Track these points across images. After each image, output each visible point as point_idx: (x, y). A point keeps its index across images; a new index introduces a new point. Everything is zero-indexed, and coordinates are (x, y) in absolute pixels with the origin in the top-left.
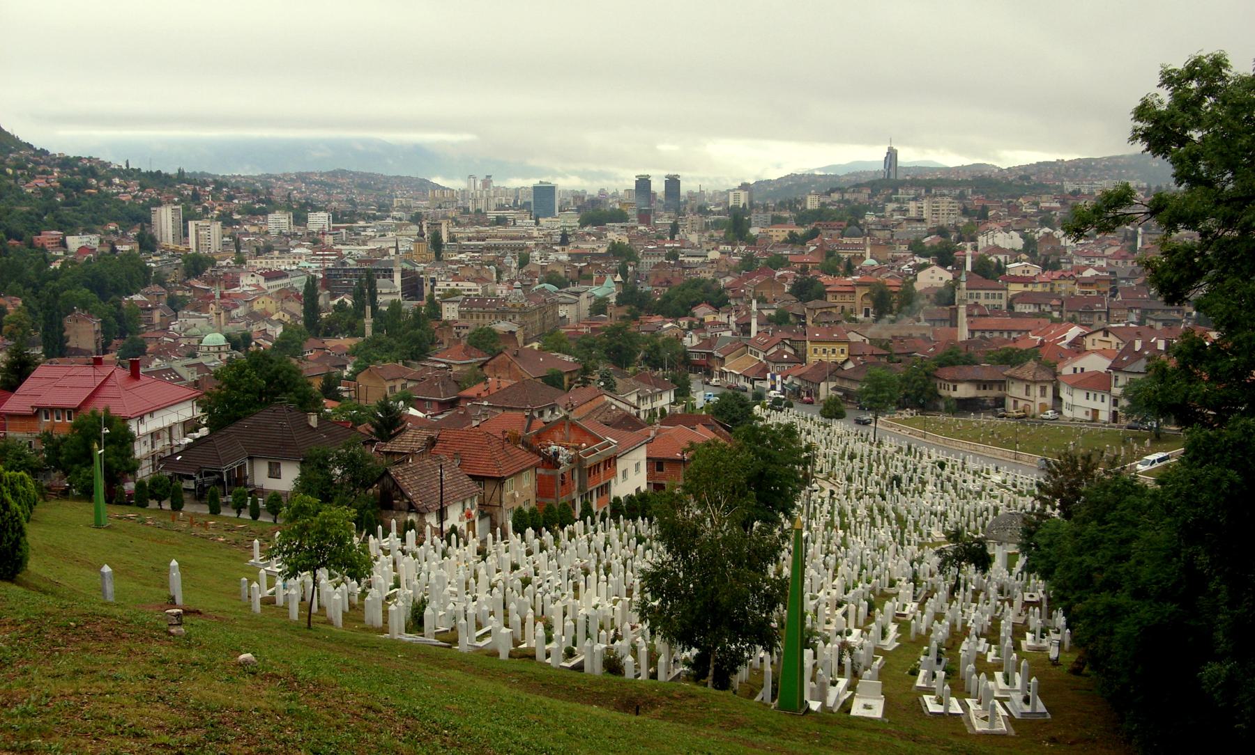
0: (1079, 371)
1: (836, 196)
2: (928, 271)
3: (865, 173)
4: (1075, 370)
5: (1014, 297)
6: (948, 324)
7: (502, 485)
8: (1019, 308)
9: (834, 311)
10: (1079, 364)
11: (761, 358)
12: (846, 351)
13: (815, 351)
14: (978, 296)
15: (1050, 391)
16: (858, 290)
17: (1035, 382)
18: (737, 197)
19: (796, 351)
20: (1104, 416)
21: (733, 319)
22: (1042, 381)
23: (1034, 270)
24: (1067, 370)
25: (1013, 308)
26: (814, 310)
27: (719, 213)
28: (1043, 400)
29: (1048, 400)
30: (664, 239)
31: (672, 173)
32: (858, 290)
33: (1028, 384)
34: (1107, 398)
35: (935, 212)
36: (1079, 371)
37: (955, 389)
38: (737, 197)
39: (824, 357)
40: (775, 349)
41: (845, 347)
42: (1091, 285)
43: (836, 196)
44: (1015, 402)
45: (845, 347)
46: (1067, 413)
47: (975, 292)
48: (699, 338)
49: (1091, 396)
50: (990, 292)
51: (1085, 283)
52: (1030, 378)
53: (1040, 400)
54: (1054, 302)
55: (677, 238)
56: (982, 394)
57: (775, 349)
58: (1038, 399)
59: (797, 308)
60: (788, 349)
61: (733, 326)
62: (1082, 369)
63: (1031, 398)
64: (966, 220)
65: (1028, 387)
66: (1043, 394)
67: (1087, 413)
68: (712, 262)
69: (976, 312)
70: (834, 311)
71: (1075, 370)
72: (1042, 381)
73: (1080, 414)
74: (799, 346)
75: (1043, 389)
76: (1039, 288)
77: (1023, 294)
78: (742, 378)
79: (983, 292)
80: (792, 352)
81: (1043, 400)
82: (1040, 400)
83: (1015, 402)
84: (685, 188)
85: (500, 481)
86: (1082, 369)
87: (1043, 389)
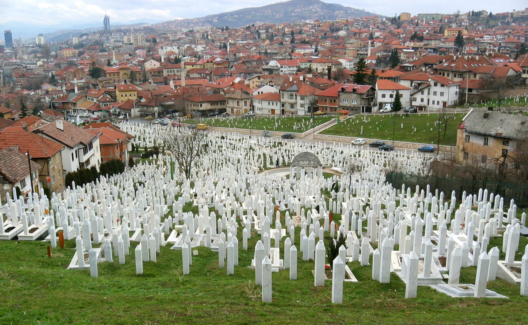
0: (260, 93)
1: (85, 37)
2: (149, 62)
3: (76, 30)
4: (259, 93)
5: (189, 72)
6: (163, 84)
7: (48, 163)
8: (192, 76)
9: (111, 81)
10: (260, 90)
11: (95, 100)
12: (136, 95)
13: (122, 96)
14: (174, 71)
15: (248, 103)
16: (120, 71)
17: (242, 99)
18: (39, 39)
19: (111, 97)
20: (278, 112)
21: (64, 88)
22: (245, 99)
23: (194, 60)
24: (255, 93)
25: (189, 76)
26: (102, 81)
27: (32, 47)
28: (245, 107)
29: (248, 107)
30: (11, 58)
31: (7, 30)
32: (120, 71)
33: (238, 101)
34: (279, 103)
35: (136, 40)
36: (260, 93)
37: (201, 106)
38: (39, 39)
39: (130, 98)
40: (102, 96)
41: (136, 93)
42: (221, 64)
43: (85, 37)
44: (232, 110)
45: (136, 93)
46: (257, 112)
47: (172, 70)
48: (49, 98)
49: (271, 103)
50: (169, 70)
51: (218, 64)
52: (239, 97)
53: (244, 107)
54: (207, 72)
55: (18, 57)
56: (213, 107)
57: (102, 96)
58: (243, 107)
59: (93, 81)
60: (108, 96)
61: (65, 91)
62: (262, 92)
63: (240, 107)
64: (149, 44)
65: (238, 102)
66: (246, 105)
67: (269, 111)
68: (40, 66)
69: (176, 78)
70: (111, 81)
71: (259, 93)
72: (245, 99)
73: (266, 112)
74: (113, 94)
75: (245, 103)
76: (198, 67)
77: (193, 70)
78: (87, 111)
79: (175, 70)
80: (109, 97)
81: (245, 107)
82: (244, 107)
83: (232, 110)
84: (112, 22)
85: (46, 160)
86: (262, 92)
87: (245, 103)
